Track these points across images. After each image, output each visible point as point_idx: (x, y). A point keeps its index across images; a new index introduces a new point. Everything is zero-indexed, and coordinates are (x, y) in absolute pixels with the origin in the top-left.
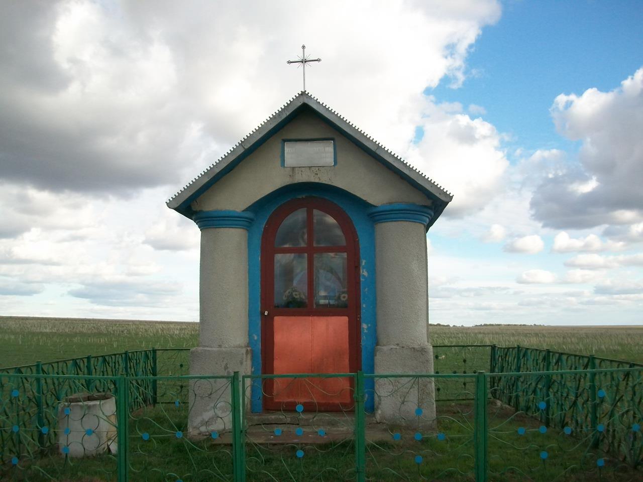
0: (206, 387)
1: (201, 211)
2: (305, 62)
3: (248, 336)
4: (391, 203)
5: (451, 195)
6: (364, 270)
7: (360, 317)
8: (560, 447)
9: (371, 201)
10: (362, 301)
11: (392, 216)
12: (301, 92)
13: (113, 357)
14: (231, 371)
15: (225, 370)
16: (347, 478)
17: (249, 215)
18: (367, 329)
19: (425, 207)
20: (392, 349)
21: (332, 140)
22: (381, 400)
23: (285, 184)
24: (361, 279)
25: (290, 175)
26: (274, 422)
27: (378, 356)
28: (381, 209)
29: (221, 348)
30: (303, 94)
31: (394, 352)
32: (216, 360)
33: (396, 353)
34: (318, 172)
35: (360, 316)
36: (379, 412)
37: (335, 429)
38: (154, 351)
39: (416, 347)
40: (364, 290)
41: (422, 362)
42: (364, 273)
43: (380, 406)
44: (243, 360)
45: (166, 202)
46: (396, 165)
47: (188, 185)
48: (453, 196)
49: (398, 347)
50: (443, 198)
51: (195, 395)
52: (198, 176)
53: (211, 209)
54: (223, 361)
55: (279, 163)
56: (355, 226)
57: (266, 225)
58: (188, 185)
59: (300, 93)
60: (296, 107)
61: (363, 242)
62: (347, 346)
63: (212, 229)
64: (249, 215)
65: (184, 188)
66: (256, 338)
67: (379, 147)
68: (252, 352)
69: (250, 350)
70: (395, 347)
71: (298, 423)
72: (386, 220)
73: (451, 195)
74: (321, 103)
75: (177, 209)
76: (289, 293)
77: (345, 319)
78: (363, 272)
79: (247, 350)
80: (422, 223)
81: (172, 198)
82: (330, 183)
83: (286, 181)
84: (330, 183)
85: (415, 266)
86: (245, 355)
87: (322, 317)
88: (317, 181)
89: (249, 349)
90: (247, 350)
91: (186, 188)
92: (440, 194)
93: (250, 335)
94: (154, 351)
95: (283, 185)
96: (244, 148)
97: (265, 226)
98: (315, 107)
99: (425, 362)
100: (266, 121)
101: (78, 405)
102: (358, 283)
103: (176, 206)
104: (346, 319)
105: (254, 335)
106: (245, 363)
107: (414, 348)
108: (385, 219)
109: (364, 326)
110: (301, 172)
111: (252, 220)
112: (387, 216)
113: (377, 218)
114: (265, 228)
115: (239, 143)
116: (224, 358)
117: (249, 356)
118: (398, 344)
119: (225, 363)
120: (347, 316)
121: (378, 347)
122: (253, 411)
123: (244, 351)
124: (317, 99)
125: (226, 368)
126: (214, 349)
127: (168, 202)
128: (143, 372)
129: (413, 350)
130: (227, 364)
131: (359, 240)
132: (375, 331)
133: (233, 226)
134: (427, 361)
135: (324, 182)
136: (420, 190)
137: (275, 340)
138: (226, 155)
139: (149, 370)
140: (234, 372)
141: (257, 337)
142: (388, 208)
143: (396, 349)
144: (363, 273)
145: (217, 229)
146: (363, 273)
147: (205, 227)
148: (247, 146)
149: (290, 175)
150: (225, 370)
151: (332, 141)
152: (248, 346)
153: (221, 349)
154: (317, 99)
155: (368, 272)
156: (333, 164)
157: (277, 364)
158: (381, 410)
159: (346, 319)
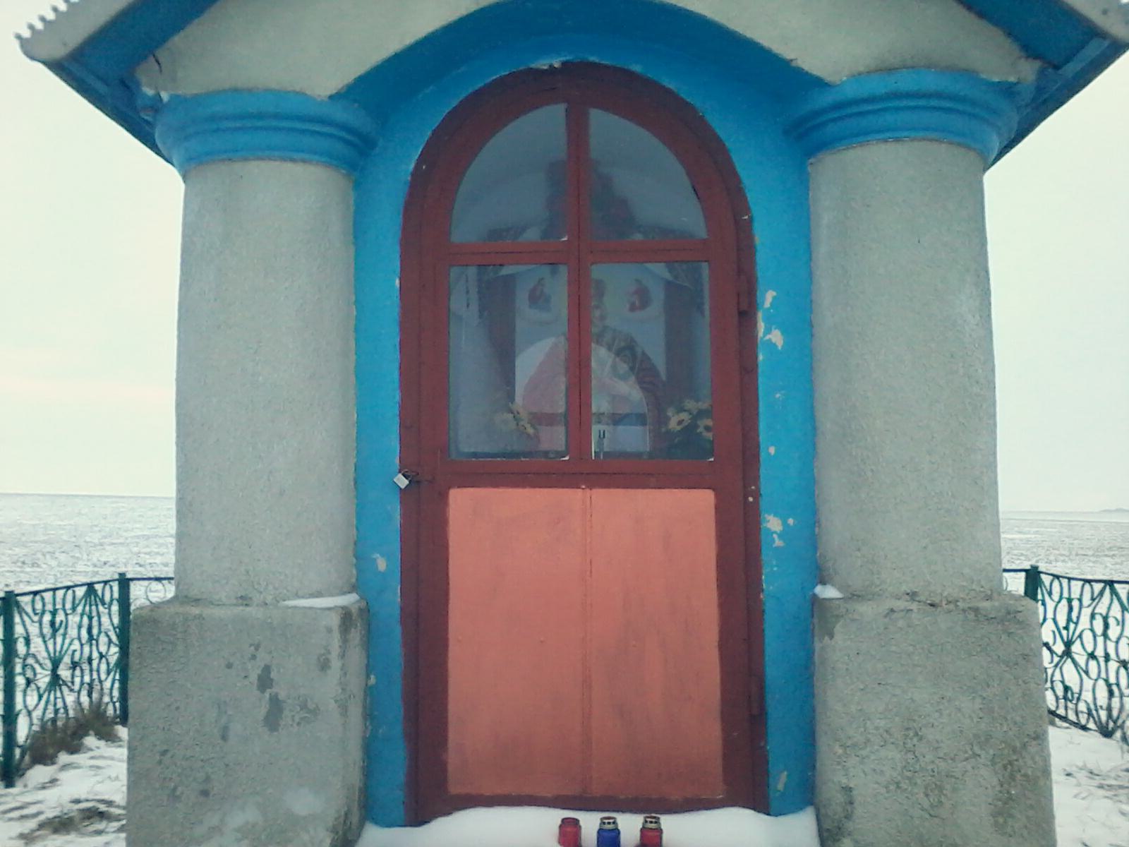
0: (189, 753)
10: (763, 438)
11: (889, 118)
13: (48, 596)
15: (263, 691)
18: (780, 536)
22: (851, 803)
28: (850, 92)
35: (758, 489)
38: (124, 582)
43: (850, 825)
44: (329, 652)
45: (19, 37)
49: (914, 606)
66: (382, 565)
72: (861, 136)
75: (59, 67)
77: (703, 501)
86: (336, 636)
94: (124, 582)
102: (748, 370)
103: (60, 52)
104: (705, 499)
106: (336, 664)
109: (769, 525)
113: (832, 129)
114: (416, 173)
117: (356, 636)
127: (27, 34)
129: (971, 616)
130: (267, 669)
131: (751, 221)
132: (814, 542)
141: (386, 563)
142: (878, 86)
144: (768, 337)
159: (705, 499)
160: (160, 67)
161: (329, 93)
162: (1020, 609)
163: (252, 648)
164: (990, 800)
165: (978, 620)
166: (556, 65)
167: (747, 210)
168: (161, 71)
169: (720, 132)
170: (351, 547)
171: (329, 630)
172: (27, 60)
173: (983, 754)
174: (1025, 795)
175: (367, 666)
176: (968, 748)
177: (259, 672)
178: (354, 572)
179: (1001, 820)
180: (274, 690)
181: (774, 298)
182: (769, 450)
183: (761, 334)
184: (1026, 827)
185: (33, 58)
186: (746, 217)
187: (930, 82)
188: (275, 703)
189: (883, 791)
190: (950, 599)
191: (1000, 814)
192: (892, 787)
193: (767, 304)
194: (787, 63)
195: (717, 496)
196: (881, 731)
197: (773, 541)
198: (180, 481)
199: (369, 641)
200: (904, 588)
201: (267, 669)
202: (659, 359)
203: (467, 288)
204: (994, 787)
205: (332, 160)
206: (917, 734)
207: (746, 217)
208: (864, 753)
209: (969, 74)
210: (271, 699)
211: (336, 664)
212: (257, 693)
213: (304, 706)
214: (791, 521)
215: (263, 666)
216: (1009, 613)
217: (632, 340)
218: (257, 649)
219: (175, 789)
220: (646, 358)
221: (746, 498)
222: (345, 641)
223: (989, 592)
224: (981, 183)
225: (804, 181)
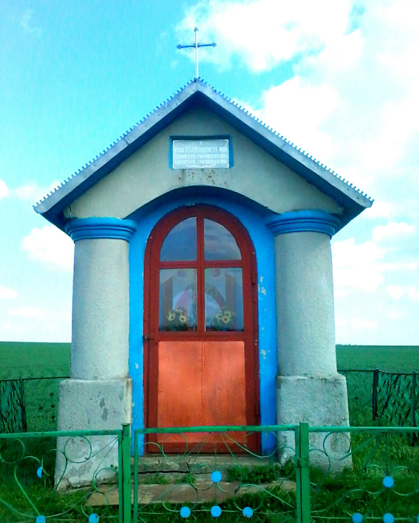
3: (128, 365)
5: (371, 200)
6: (263, 288)
7: (258, 342)
14: (108, 408)
15: (101, 407)
17: (130, 223)
18: (266, 356)
20: (299, 380)
23: (174, 188)
25: (180, 178)
28: (281, 218)
29: (97, 380)
31: (302, 383)
32: (90, 395)
33: (304, 384)
34: (211, 175)
36: (285, 456)
38: (22, 381)
39: (328, 378)
41: (335, 396)
45: (34, 206)
48: (374, 200)
49: (306, 378)
50: (361, 203)
51: (67, 459)
52: (72, 175)
53: (87, 217)
54: (99, 396)
55: (166, 164)
57: (150, 235)
63: (86, 240)
64: (130, 223)
65: (55, 189)
66: (137, 367)
69: (131, 381)
70: (302, 377)
71: (187, 470)
75: (46, 215)
78: (261, 290)
79: (128, 382)
82: (225, 187)
83: (176, 185)
85: (323, 282)
86: (125, 389)
88: (210, 184)
89: (129, 380)
90: (128, 382)
91: (57, 189)
93: (131, 364)
96: (127, 143)
99: (338, 396)
102: (255, 302)
103: (45, 210)
106: (125, 398)
107: (325, 380)
108: (288, 229)
111: (134, 230)
112: (292, 225)
115: (121, 137)
116: (100, 393)
117: (130, 389)
118: (305, 375)
120: (243, 341)
121: (282, 377)
128: (9, 404)
129: (324, 381)
130: (103, 400)
135: (218, 186)
136: (330, 195)
137: (160, 369)
139: (16, 401)
140: (123, 426)
141: (139, 366)
142: (294, 215)
143: (304, 380)
144: (262, 292)
145: (94, 240)
146: (262, 292)
147: (79, 238)
148: (131, 140)
150: (101, 407)
151: (227, 140)
152: (128, 377)
153: (97, 381)
156: (228, 166)
160: (71, 209)
162: (339, 379)
163: (99, 393)
164: (330, 440)
165: (326, 383)
167: (254, 251)
168: (71, 211)
169: (245, 225)
171: (123, 387)
172: (34, 210)
174: (341, 438)
175: (132, 399)
176: (323, 423)
177: (100, 401)
180: (105, 407)
183: (259, 291)
184: (341, 449)
185: (35, 210)
186: (254, 253)
188: (106, 411)
190: (317, 376)
191: (333, 445)
195: (245, 343)
196: (296, 418)
201: (103, 400)
202: (224, 295)
203: (328, 456)
206: (307, 419)
207: (254, 253)
210: (104, 409)
212: (100, 407)
213: (115, 412)
214: (269, 351)
215: (101, 399)
216: (335, 380)
217: (214, 287)
218: (100, 394)
220: (219, 293)
221: (254, 344)
222: (127, 390)
223: (330, 374)
224: (330, 242)
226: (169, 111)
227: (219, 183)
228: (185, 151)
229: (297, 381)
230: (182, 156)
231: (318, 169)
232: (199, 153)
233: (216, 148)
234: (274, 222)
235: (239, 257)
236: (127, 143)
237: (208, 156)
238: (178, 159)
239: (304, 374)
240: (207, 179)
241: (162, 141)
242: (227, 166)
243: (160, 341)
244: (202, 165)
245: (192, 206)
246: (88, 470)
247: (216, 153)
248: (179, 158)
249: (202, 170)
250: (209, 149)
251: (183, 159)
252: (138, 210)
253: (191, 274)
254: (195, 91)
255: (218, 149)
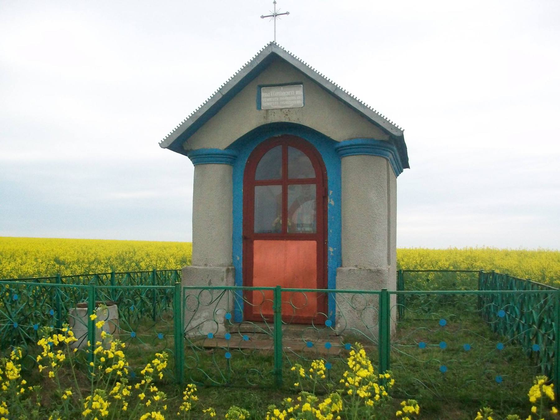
1: (191, 150)
2: (276, 16)
4: (351, 139)
5: (402, 130)
6: (331, 200)
8: (211, 294)
9: (334, 137)
11: (352, 150)
12: (270, 42)
16: (38, 313)
17: (234, 152)
18: (333, 252)
19: (382, 141)
20: (350, 270)
21: (301, 84)
24: (329, 208)
25: (264, 117)
26: (248, 331)
27: (338, 276)
28: (340, 145)
30: (272, 44)
36: (339, 326)
37: (299, 339)
39: (372, 268)
40: (330, 217)
42: (331, 202)
45: (159, 143)
46: (352, 103)
47: (177, 128)
48: (404, 130)
49: (356, 269)
53: (200, 148)
55: (254, 107)
56: (324, 160)
57: (248, 161)
58: (177, 128)
59: (269, 43)
60: (265, 56)
61: (330, 177)
62: (314, 266)
64: (234, 152)
65: (173, 130)
66: (238, 258)
67: (337, 88)
68: (235, 270)
70: (353, 268)
73: (402, 130)
74: (287, 52)
76: (277, 220)
78: (330, 201)
80: (384, 158)
81: (164, 139)
83: (262, 122)
84: (298, 123)
87: (294, 241)
88: (287, 121)
92: (392, 129)
93: (233, 257)
95: (259, 125)
96: (222, 94)
97: (247, 162)
98: (281, 55)
100: (240, 70)
101: (84, 310)
105: (237, 256)
107: (370, 270)
109: (330, 250)
110: (273, 114)
113: (342, 152)
114: (247, 163)
116: (208, 275)
117: (231, 274)
118: (356, 266)
119: (209, 279)
120: (316, 240)
122: (234, 320)
123: (224, 269)
124: (284, 48)
125: (210, 283)
126: (201, 267)
127: (161, 142)
129: (369, 271)
130: (210, 281)
132: (340, 254)
133: (210, 163)
134: (382, 281)
138: (208, 101)
141: (239, 258)
144: (330, 203)
149: (264, 117)
151: (302, 85)
154: (284, 48)
155: (334, 202)
156: (303, 106)
157: (255, 281)
158: (340, 324)
161: (224, 148)
166: (280, 136)
167: (326, 170)
170: (231, 254)
173: (371, 304)
178: (232, 260)
179: (375, 321)
181: (332, 193)
182: (330, 231)
183: (329, 201)
187: (360, 142)
189: (347, 313)
192: (349, 312)
193: (330, 194)
194: (329, 137)
197: (330, 253)
198: (193, 238)
199: (235, 276)
200: (355, 264)
201: (210, 281)
204: (373, 313)
205: (227, 163)
208: (343, 303)
209: (372, 139)
211: (225, 280)
219: (191, 307)
221: (324, 243)
225: (340, 163)
226: (252, 68)
227: (293, 119)
228: (270, 95)
229: (349, 271)
230: (268, 100)
231: (362, 107)
232: (281, 97)
233: (293, 92)
234: (338, 148)
235: (313, 176)
236: (222, 94)
237: (287, 98)
238: (265, 102)
239: (355, 266)
240: (285, 117)
241: (251, 90)
242: (302, 105)
243: (254, 240)
244: (283, 105)
245: (279, 137)
246: (201, 329)
247: (293, 96)
248: (266, 101)
249: (281, 109)
250: (288, 93)
251: (269, 102)
252: (234, 142)
253: (277, 190)
254: (271, 52)
255: (295, 92)
